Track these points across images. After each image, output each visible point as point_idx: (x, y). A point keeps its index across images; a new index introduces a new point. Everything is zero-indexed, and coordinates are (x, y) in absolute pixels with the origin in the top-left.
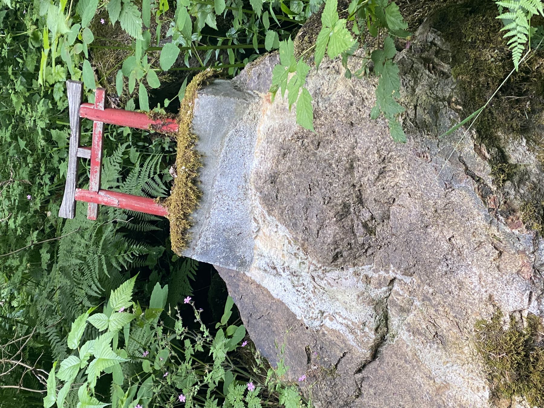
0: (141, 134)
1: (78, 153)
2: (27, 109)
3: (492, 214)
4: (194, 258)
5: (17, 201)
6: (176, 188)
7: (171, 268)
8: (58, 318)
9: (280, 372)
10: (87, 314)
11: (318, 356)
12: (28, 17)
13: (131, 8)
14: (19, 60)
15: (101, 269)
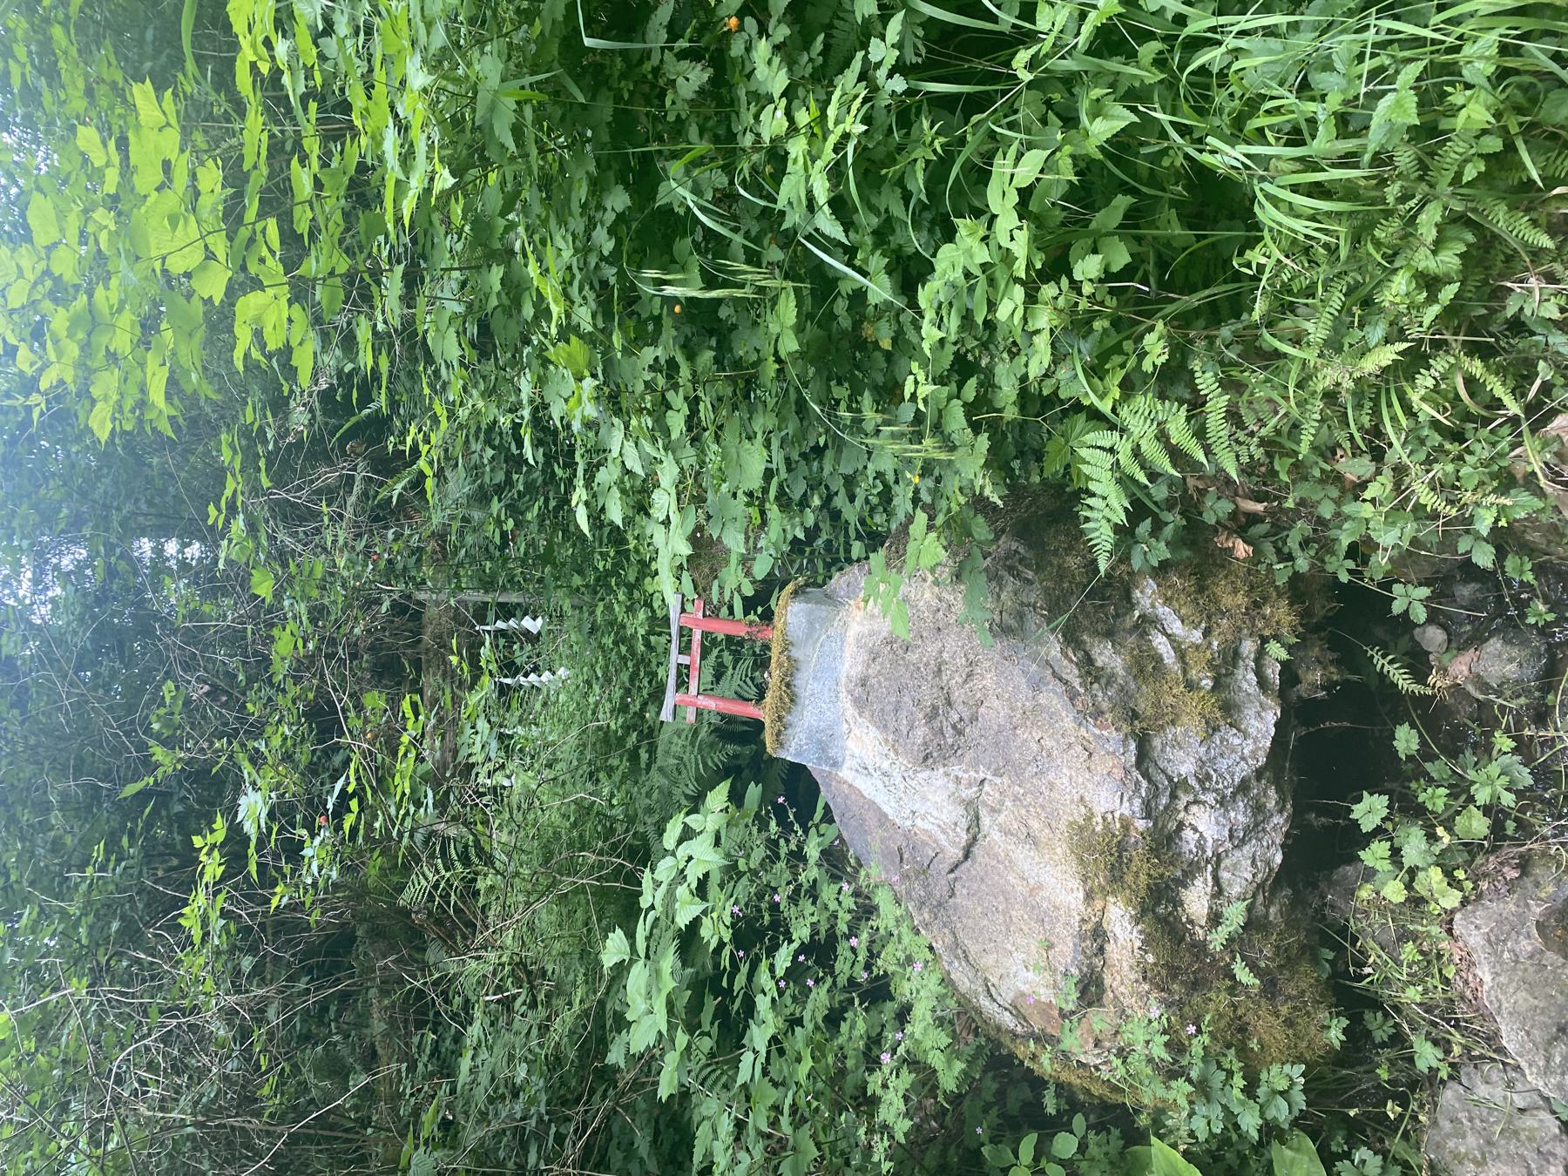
3: (1081, 716)
9: (874, 872)
11: (911, 857)
15: (697, 768)
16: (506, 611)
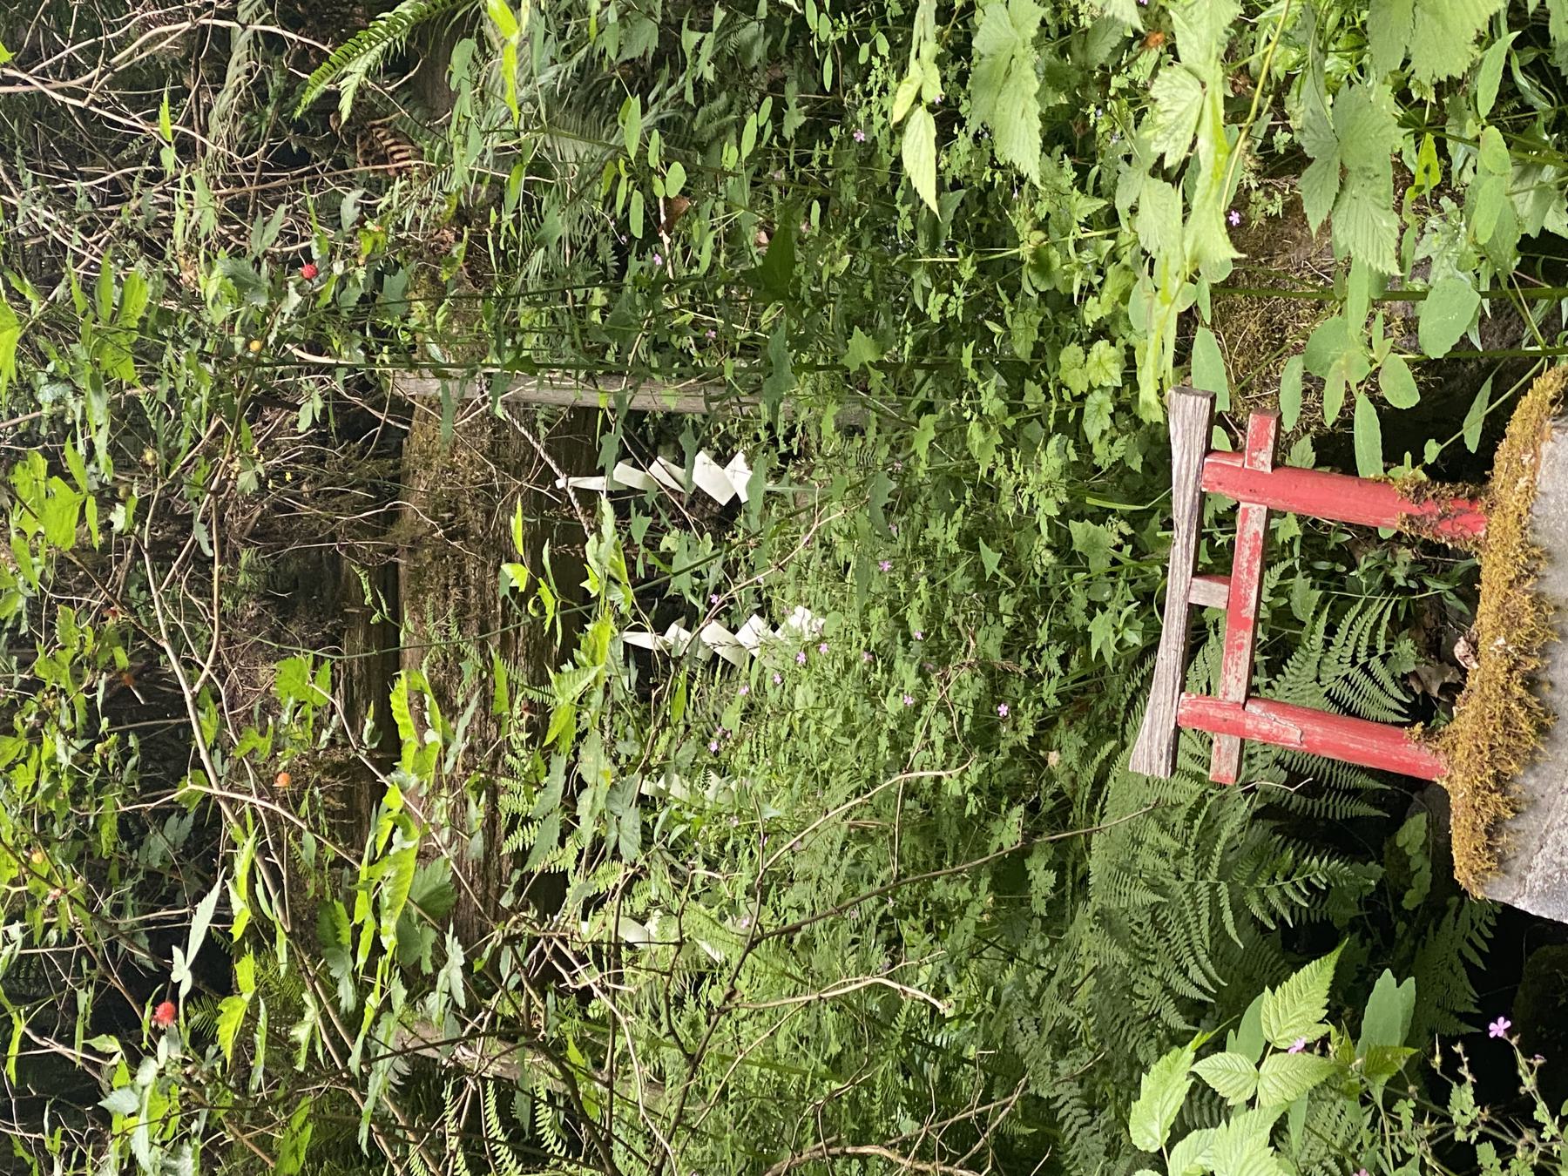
0: (1326, 539)
1: (1192, 593)
2: (1009, 462)
4: (1521, 905)
5: (967, 720)
6: (1475, 700)
7: (1401, 927)
8: (1087, 1057)
10: (1189, 1052)
12: (1022, 209)
13: (1368, 183)
14: (991, 325)
16: (651, 437)
